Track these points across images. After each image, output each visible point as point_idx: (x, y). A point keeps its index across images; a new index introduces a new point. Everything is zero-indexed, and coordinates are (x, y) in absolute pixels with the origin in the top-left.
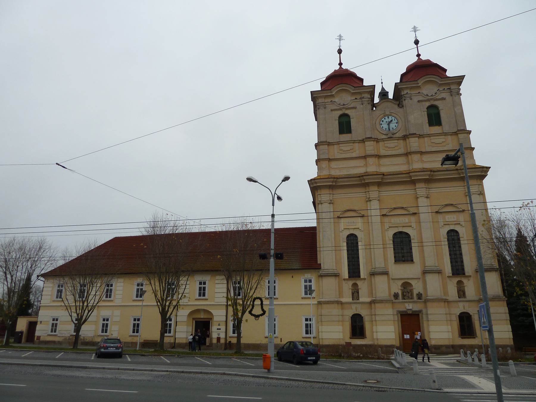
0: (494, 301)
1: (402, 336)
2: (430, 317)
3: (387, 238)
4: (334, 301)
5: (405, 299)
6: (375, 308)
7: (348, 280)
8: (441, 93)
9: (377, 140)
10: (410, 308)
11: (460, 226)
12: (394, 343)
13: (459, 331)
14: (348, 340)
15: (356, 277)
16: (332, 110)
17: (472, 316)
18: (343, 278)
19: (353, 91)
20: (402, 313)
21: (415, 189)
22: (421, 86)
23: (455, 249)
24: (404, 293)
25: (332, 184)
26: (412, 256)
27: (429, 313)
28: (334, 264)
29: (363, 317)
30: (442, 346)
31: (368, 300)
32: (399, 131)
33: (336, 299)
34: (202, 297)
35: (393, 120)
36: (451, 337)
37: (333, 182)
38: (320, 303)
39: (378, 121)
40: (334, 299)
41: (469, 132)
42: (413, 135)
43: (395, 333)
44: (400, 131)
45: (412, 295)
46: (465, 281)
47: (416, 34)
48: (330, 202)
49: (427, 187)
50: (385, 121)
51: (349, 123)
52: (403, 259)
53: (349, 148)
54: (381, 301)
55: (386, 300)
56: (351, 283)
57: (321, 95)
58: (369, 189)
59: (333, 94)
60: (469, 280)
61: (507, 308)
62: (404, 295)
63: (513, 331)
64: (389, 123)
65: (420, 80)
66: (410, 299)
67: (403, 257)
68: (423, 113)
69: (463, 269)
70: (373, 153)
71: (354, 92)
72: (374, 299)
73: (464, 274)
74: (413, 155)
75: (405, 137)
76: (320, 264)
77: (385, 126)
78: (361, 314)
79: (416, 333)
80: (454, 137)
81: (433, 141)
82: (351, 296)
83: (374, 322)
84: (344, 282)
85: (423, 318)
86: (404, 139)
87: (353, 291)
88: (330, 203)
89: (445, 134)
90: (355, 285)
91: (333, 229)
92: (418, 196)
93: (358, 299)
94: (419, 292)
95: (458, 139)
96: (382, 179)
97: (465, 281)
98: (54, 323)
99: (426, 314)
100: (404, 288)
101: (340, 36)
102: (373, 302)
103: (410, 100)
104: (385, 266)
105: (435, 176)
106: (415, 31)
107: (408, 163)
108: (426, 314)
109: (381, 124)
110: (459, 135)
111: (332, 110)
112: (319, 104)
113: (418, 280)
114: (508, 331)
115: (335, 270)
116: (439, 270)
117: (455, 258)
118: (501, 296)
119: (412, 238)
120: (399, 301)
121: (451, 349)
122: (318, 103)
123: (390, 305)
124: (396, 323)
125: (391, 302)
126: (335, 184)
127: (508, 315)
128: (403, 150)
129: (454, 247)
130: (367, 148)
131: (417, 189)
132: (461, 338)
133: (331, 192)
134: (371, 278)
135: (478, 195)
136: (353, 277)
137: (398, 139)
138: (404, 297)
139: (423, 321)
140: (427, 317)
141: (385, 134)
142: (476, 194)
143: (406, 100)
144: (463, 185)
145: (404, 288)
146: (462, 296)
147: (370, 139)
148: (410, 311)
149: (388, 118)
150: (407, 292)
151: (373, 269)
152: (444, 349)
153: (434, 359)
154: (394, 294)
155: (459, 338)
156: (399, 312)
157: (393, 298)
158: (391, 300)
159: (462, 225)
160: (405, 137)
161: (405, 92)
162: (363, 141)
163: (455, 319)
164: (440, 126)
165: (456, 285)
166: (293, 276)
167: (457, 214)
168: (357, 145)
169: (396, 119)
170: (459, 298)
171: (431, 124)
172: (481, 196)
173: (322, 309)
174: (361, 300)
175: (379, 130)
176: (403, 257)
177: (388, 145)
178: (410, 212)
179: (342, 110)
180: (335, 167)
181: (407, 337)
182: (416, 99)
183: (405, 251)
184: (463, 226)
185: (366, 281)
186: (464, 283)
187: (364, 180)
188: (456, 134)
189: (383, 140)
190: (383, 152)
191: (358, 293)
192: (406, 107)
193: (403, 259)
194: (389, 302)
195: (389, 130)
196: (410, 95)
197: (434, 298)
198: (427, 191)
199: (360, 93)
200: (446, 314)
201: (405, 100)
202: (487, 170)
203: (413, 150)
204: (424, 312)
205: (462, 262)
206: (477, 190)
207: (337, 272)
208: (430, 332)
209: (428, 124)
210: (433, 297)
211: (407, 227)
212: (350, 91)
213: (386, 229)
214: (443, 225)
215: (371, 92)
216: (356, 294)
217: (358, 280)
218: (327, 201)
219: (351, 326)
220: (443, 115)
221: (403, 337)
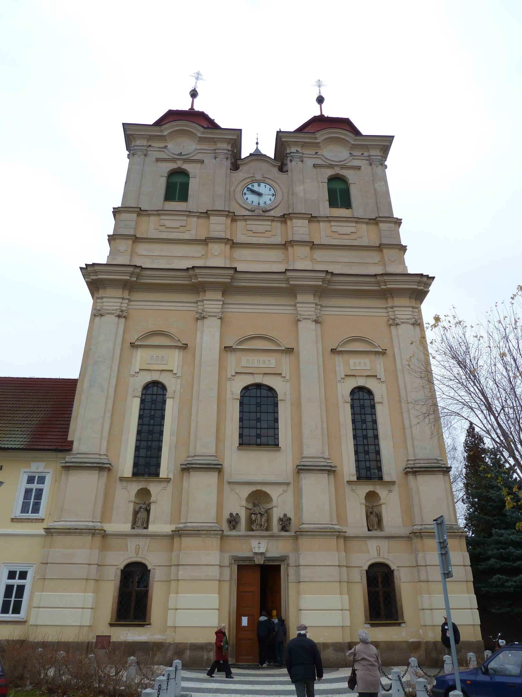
2: (303, 572)
3: (229, 396)
4: (84, 527)
5: (253, 530)
7: (132, 481)
8: (353, 159)
10: (261, 551)
13: (365, 607)
14: (104, 630)
15: (150, 475)
16: (158, 160)
17: (396, 573)
18: (119, 475)
19: (202, 134)
20: (241, 563)
21: (295, 305)
22: (320, 144)
26: (276, 437)
27: (302, 562)
28: (104, 443)
29: (149, 571)
31: (168, 529)
32: (276, 207)
36: (348, 623)
38: (49, 532)
39: (239, 188)
40: (86, 523)
41: (398, 222)
43: (219, 613)
45: (269, 520)
48: (118, 313)
49: (318, 303)
51: (185, 187)
53: (177, 224)
55: (208, 529)
56: (135, 487)
57: (142, 133)
59: (161, 129)
60: (390, 491)
61: (467, 555)
62: (252, 519)
63: (481, 608)
66: (263, 530)
67: (258, 436)
68: (321, 184)
69: (380, 469)
70: (222, 235)
71: (203, 136)
72: (182, 526)
73: (381, 478)
74: (295, 248)
75: (284, 218)
76: (72, 442)
81: (334, 229)
82: (130, 518)
84: (119, 486)
85: (288, 575)
86: (283, 221)
87: (138, 506)
88: (119, 316)
89: (358, 220)
90: (144, 493)
91: (115, 369)
93: (145, 525)
94: (285, 515)
95: (379, 230)
96: (232, 278)
97: (382, 492)
100: (255, 505)
102: (178, 533)
103: (300, 162)
104: (216, 453)
105: (335, 284)
106: (319, 86)
107: (286, 260)
109: (245, 194)
110: (381, 225)
111: (158, 160)
113: (285, 487)
114: (471, 609)
116: (330, 466)
118: (454, 526)
119: (280, 397)
122: (135, 146)
124: (226, 586)
126: (135, 279)
127: (469, 569)
128: (280, 239)
131: (298, 305)
133: (126, 295)
134: (183, 477)
135: (412, 327)
136: (143, 475)
137: (273, 219)
138: (251, 524)
140: (298, 574)
141: (250, 209)
142: (407, 323)
144: (385, 306)
145: (254, 506)
147: (218, 213)
148: (259, 557)
150: (260, 513)
151: (190, 459)
154: (228, 516)
156: (236, 559)
157: (225, 526)
158: (218, 529)
159: (380, 379)
160: (284, 218)
161: (293, 150)
162: (207, 214)
164: (348, 209)
165: (364, 501)
167: (372, 357)
169: (272, 189)
170: (369, 530)
171: (333, 203)
172: (418, 328)
174: (153, 528)
176: (258, 436)
177: (253, 228)
179: (176, 163)
180: (145, 253)
181: (263, 618)
182: (310, 162)
184: (382, 380)
185: (171, 485)
186: (380, 497)
187: (196, 276)
188: (375, 221)
189: (244, 218)
190: (240, 238)
191: (148, 511)
192: (292, 172)
194: (215, 534)
196: (301, 155)
198: (318, 311)
200: (339, 566)
201: (291, 161)
202: (429, 281)
203: (297, 238)
204: (292, 560)
205: (378, 453)
206: (411, 316)
207: (105, 461)
208: (301, 610)
209: (328, 202)
213: (229, 376)
215: (233, 141)
216: (142, 515)
217: (152, 481)
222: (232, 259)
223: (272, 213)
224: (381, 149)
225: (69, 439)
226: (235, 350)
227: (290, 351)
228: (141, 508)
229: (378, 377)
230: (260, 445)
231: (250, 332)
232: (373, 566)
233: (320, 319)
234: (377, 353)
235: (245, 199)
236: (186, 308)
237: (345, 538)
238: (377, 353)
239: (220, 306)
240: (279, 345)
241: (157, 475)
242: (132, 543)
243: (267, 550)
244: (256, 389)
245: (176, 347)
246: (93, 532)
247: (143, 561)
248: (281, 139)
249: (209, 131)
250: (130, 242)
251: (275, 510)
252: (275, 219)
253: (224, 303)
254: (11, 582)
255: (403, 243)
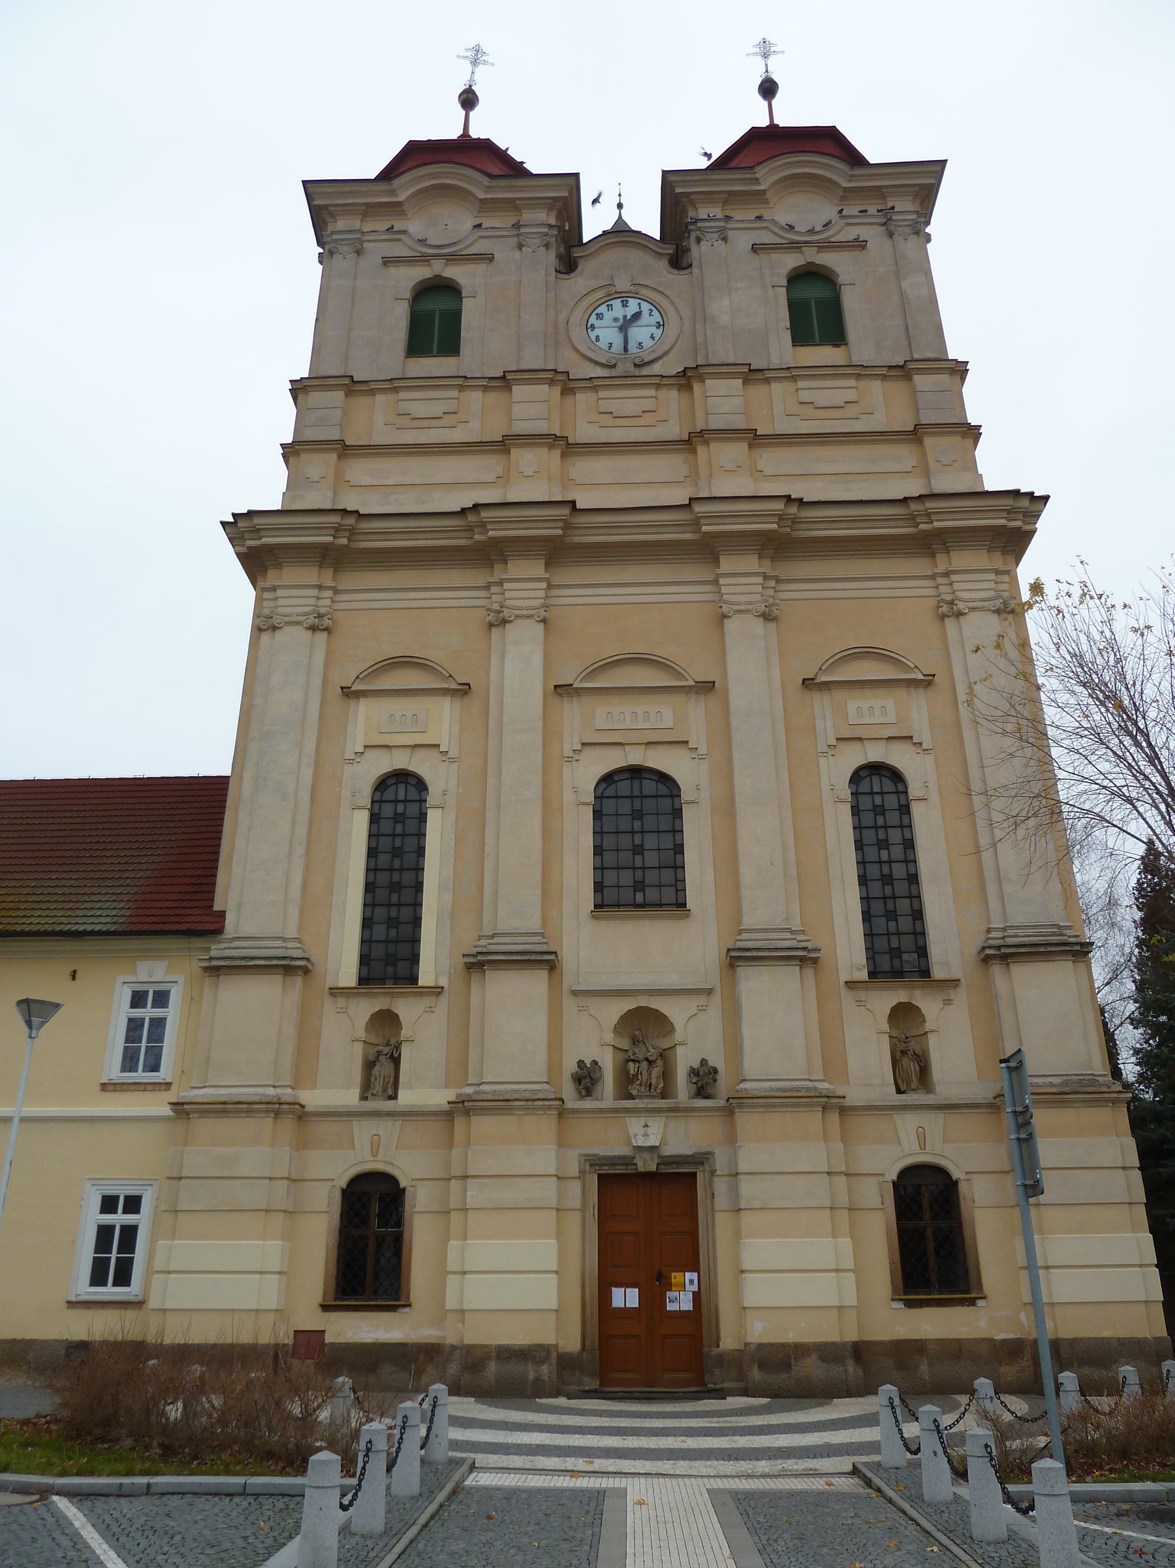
0: (1065, 1104)
1: (596, 1292)
2: (747, 1187)
3: (568, 797)
4: (256, 1099)
6: (468, 1143)
7: (358, 995)
8: (848, 224)
9: (567, 384)
10: (649, 1144)
11: (913, 748)
12: (543, 1333)
13: (892, 1263)
14: (310, 1318)
15: (398, 980)
16: (387, 262)
17: (963, 1188)
18: (330, 983)
19: (487, 192)
20: (606, 1170)
22: (768, 195)
23: (884, 855)
24: (631, 1064)
25: (331, 539)
26: (679, 885)
27: (743, 1166)
28: (294, 913)
29: (404, 1190)
30: (800, 1350)
31: (440, 1098)
33: (271, 1091)
34: (141, 1075)
35: (645, 313)
37: (337, 530)
38: (181, 1109)
40: (261, 1090)
41: (960, 370)
42: (724, 370)
44: (671, 354)
45: (667, 1075)
46: (928, 1005)
47: (766, 65)
48: (312, 620)
49: (770, 573)
50: (608, 316)
51: (453, 320)
52: (639, 897)
53: (437, 408)
54: (503, 1105)
56: (364, 1009)
57: (350, 201)
58: (506, 572)
60: (948, 1002)
64: (625, 326)
65: (767, 169)
67: (639, 886)
68: (771, 292)
69: (922, 951)
71: (489, 196)
72: (469, 1090)
73: (925, 973)
75: (686, 379)
76: (222, 915)
77: (607, 334)
78: (396, 1173)
79: (676, 1277)
80: (897, 388)
81: (805, 396)
82: (357, 1076)
83: (455, 1217)
84: (330, 1007)
86: (681, 385)
88: (313, 629)
89: (861, 372)
90: (386, 1020)
92: (725, 608)
93: (390, 1092)
94: (703, 1062)
95: (914, 392)
96: (567, 526)
97: (928, 1005)
98: (113, 1227)
99: (730, 1175)
100: (635, 1041)
101: (477, 50)
102: (463, 1108)
108: (730, 1175)
109: (593, 327)
110: (917, 378)
111: (387, 262)
112: (335, 237)
113: (702, 1000)
115: (289, 945)
116: (804, 949)
117: (885, 898)
120: (602, 1105)
121: (851, 1368)
123: (546, 1125)
125: (550, 1108)
126: (344, 541)
127: (1137, 1176)
129: (884, 844)
130: (516, 409)
132: (901, 1305)
133: (327, 578)
136: (381, 980)
137: (661, 382)
138: (626, 1083)
139: (713, 1210)
140: (735, 1192)
141: (605, 362)
142: (982, 609)
143: (702, 243)
144: (929, 573)
146: (914, 1085)
147: (531, 375)
148: (647, 1156)
149: (625, 304)
150: (647, 1059)
151: (483, 942)
152: (812, 1368)
153: (742, 1442)
154: (574, 1068)
155: (896, 1305)
156: (594, 1162)
157: (568, 1090)
159: (921, 744)
160: (686, 379)
161: (702, 213)
162: (504, 382)
163: (876, 1202)
165: (885, 1027)
166: (75, 972)
167: (901, 693)
168: (476, 397)
169: (655, 312)
170: (899, 1091)
171: (801, 335)
173: (186, 1144)
174: (407, 1097)
175: (583, 348)
176: (639, 886)
177: (615, 406)
178: (685, 679)
180: (368, 481)
181: (626, 1298)
182: (742, 241)
183: (651, 859)
184: (925, 746)
187: (483, 525)
188: (903, 371)
189: (592, 384)
190: (584, 432)
191: (396, 1061)
193: (639, 897)
195: (626, 349)
197: (772, 1089)
199: (513, 205)
200: (828, 1173)
201: (699, 240)
202: (1035, 507)
203: (715, 423)
204: (721, 1163)
205: (918, 915)
206: (992, 594)
208: (743, 1272)
209: (788, 334)
210: (767, 1084)
211: (666, 748)
212: (473, 195)
213: (567, 752)
214: (834, 742)
216: (383, 1069)
218: (301, 618)
219: (334, 1241)
220: (852, 303)
221: (604, 1297)
222: (566, 481)
223: (657, 368)
224: (915, 196)
225: (217, 907)
226: (579, 692)
227: (706, 687)
228: (379, 1053)
229: (915, 740)
230: (642, 906)
231: (614, 649)
232: (906, 1173)
233: (776, 612)
234: (911, 683)
235: (594, 339)
236: (463, 603)
237: (843, 1110)
238: (911, 683)
239: (542, 594)
240: (678, 674)
241: (413, 979)
242: (363, 1131)
243: (663, 1140)
244: (632, 779)
245: (445, 692)
246: (276, 1108)
247: (389, 1169)
248: (673, 189)
249: (503, 182)
250: (333, 457)
251: (679, 1050)
252: (665, 381)
253: (550, 586)
254: (108, 1219)
255: (972, 420)
